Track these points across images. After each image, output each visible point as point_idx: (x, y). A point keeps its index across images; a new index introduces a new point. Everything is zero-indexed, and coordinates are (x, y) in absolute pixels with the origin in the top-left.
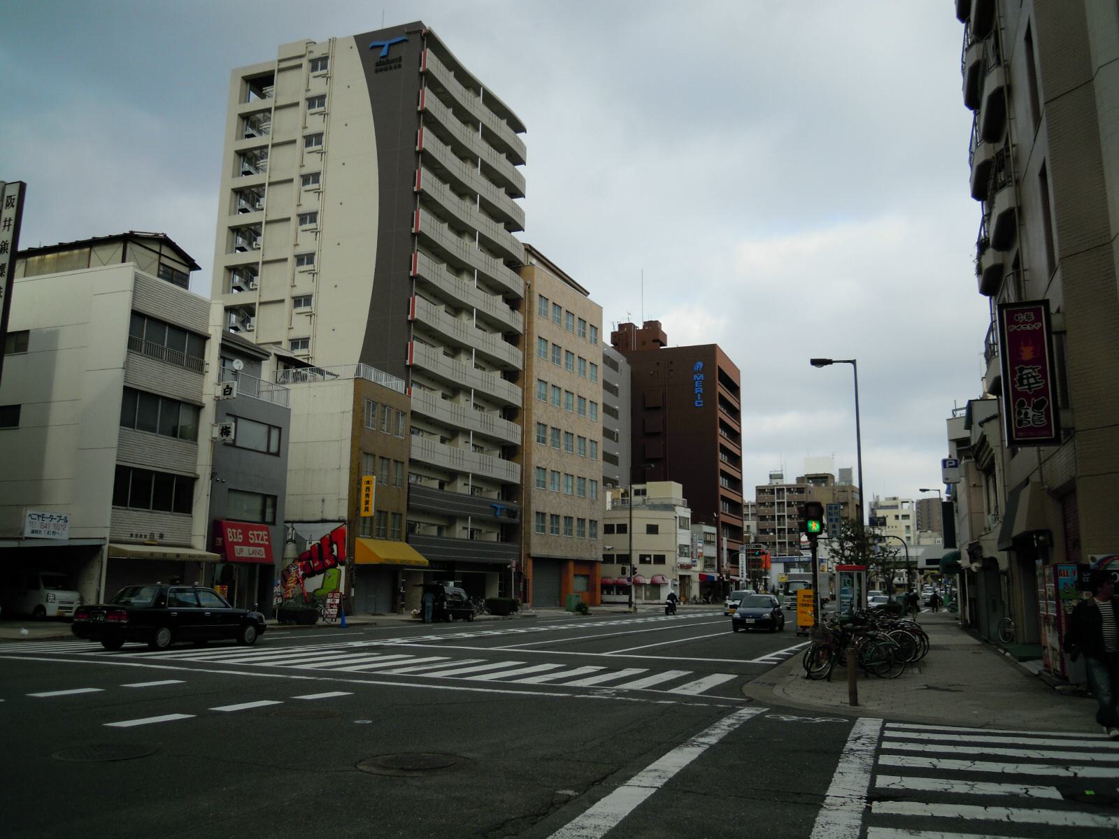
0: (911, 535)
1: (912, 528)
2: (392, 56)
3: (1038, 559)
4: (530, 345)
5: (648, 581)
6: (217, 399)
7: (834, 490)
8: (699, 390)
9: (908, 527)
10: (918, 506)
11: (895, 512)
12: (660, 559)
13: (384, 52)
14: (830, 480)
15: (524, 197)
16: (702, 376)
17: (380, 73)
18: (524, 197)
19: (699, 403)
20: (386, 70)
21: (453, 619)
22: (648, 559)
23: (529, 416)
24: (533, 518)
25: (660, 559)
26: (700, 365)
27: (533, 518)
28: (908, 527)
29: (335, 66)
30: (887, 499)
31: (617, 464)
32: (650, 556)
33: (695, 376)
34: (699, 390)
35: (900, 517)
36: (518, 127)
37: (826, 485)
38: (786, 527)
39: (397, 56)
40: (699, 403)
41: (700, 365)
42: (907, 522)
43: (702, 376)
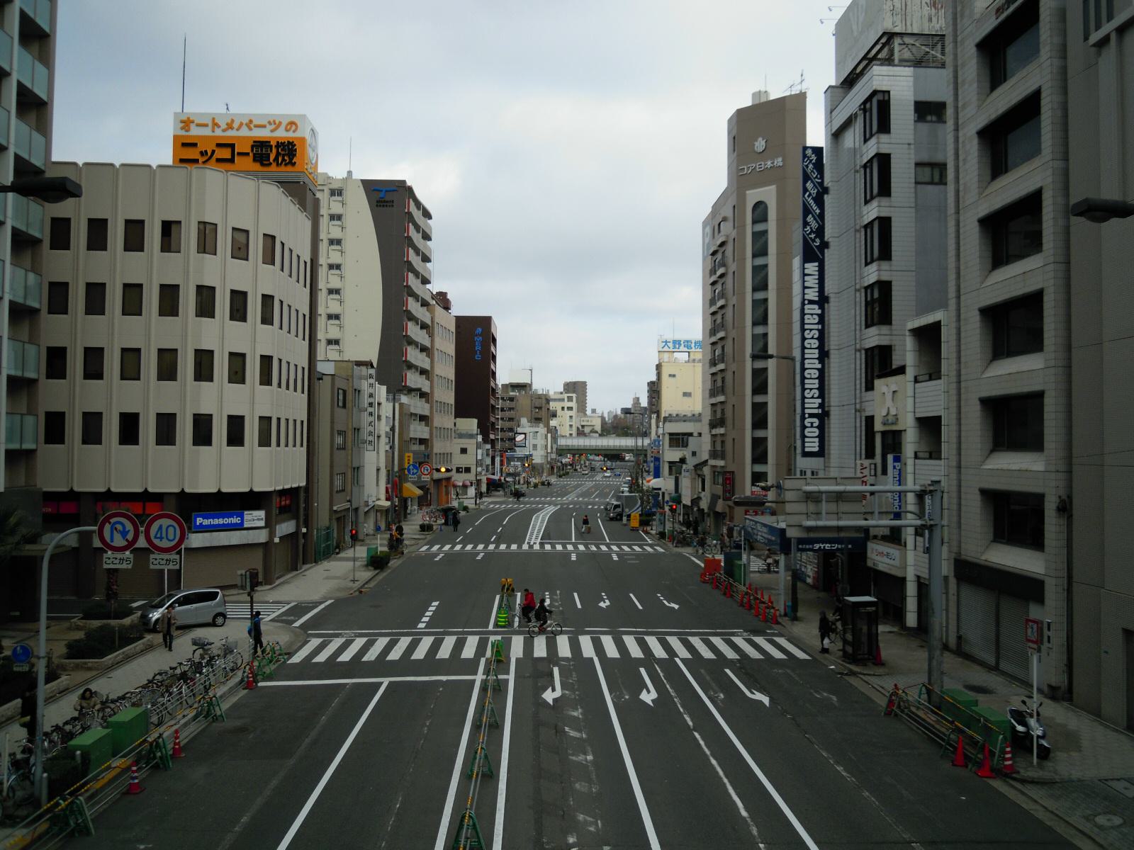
0: (573, 423)
1: (574, 418)
2: (387, 198)
3: (514, 543)
4: (433, 354)
5: (461, 484)
6: (387, 433)
7: (532, 397)
8: (478, 348)
9: (571, 417)
10: (566, 387)
11: (562, 404)
12: (468, 470)
13: (382, 195)
14: (528, 388)
15: (820, 652)
16: (481, 338)
17: (379, 208)
18: (820, 652)
19: (478, 357)
20: (383, 206)
21: (488, 489)
22: (461, 470)
23: (432, 397)
24: (434, 456)
25: (468, 470)
26: (479, 330)
27: (434, 456)
28: (571, 417)
29: (348, 195)
30: (555, 393)
31: (983, 492)
32: (462, 468)
33: (476, 338)
34: (478, 348)
35: (566, 409)
36: (427, 215)
37: (525, 393)
38: (499, 427)
39: (391, 199)
40: (478, 357)
41: (479, 330)
42: (570, 413)
43: (481, 338)
